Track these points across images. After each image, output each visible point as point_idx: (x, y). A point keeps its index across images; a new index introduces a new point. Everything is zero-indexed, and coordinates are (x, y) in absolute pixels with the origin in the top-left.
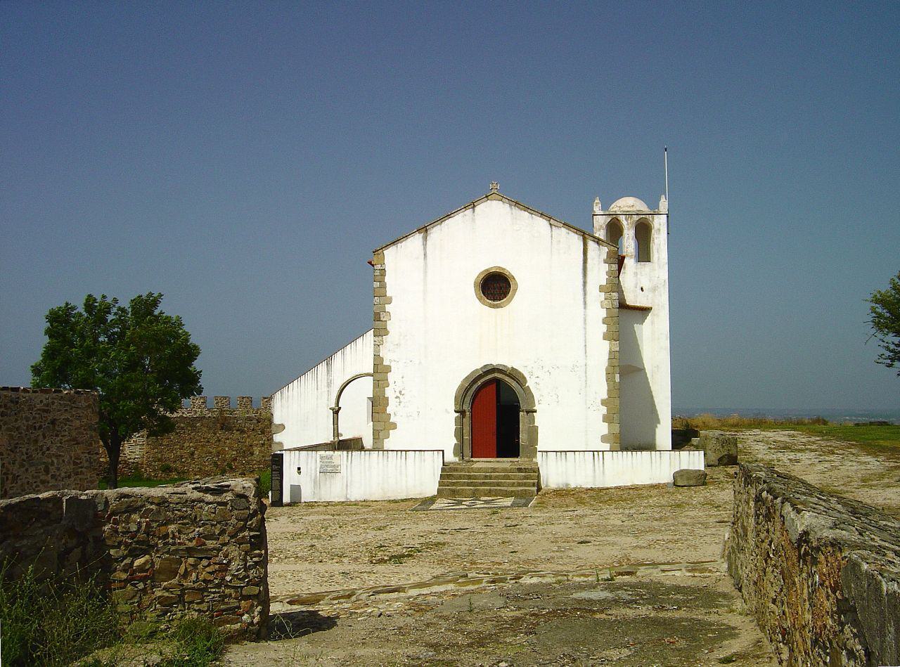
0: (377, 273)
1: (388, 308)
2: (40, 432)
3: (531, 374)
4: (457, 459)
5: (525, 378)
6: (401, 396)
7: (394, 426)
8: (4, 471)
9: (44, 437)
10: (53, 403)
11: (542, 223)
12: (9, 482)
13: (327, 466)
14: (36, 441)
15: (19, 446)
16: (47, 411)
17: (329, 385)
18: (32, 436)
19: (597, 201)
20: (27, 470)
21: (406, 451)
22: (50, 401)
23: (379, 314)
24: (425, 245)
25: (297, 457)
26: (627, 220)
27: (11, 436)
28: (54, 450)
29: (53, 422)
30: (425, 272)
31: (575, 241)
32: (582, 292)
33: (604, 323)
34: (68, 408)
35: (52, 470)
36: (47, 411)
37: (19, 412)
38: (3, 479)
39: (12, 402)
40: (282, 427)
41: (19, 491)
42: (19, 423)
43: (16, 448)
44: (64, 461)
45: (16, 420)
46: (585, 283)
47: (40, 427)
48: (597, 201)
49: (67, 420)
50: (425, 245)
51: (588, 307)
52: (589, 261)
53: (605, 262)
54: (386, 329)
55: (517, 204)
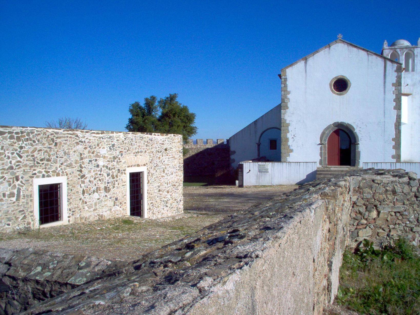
0: (283, 80)
1: (289, 96)
2: (160, 154)
3: (357, 126)
4: (321, 166)
5: (354, 128)
6: (294, 138)
7: (292, 151)
8: (148, 172)
9: (163, 156)
10: (165, 140)
11: (363, 54)
12: (150, 176)
13: (262, 169)
14: (160, 158)
15: (153, 160)
16: (163, 144)
17: (256, 132)
18: (158, 155)
19: (386, 42)
20: (156, 171)
21: (299, 162)
22: (164, 139)
23: (284, 99)
24: (306, 66)
25: (249, 165)
26: (400, 51)
27: (150, 156)
28: (166, 162)
29: (166, 150)
30: (306, 79)
31: (380, 61)
32: (383, 87)
33: (394, 101)
34: (171, 143)
35: (166, 171)
36: (163, 144)
37: (153, 144)
38: (148, 175)
39: (150, 140)
40: (234, 152)
41: (154, 180)
42: (153, 150)
43: (152, 161)
44: (170, 167)
45: (152, 148)
46: (385, 82)
47: (161, 151)
48: (386, 42)
49: (171, 148)
50: (306, 66)
51: (386, 93)
52: (387, 71)
53: (395, 71)
54: (287, 106)
55: (351, 45)
